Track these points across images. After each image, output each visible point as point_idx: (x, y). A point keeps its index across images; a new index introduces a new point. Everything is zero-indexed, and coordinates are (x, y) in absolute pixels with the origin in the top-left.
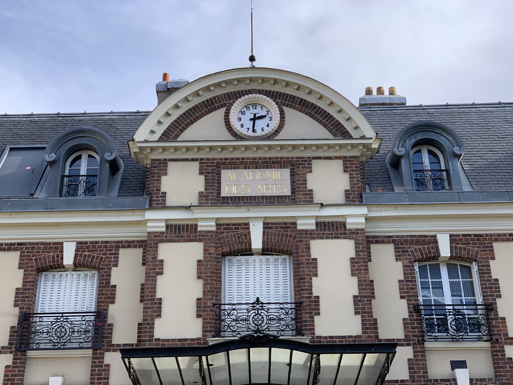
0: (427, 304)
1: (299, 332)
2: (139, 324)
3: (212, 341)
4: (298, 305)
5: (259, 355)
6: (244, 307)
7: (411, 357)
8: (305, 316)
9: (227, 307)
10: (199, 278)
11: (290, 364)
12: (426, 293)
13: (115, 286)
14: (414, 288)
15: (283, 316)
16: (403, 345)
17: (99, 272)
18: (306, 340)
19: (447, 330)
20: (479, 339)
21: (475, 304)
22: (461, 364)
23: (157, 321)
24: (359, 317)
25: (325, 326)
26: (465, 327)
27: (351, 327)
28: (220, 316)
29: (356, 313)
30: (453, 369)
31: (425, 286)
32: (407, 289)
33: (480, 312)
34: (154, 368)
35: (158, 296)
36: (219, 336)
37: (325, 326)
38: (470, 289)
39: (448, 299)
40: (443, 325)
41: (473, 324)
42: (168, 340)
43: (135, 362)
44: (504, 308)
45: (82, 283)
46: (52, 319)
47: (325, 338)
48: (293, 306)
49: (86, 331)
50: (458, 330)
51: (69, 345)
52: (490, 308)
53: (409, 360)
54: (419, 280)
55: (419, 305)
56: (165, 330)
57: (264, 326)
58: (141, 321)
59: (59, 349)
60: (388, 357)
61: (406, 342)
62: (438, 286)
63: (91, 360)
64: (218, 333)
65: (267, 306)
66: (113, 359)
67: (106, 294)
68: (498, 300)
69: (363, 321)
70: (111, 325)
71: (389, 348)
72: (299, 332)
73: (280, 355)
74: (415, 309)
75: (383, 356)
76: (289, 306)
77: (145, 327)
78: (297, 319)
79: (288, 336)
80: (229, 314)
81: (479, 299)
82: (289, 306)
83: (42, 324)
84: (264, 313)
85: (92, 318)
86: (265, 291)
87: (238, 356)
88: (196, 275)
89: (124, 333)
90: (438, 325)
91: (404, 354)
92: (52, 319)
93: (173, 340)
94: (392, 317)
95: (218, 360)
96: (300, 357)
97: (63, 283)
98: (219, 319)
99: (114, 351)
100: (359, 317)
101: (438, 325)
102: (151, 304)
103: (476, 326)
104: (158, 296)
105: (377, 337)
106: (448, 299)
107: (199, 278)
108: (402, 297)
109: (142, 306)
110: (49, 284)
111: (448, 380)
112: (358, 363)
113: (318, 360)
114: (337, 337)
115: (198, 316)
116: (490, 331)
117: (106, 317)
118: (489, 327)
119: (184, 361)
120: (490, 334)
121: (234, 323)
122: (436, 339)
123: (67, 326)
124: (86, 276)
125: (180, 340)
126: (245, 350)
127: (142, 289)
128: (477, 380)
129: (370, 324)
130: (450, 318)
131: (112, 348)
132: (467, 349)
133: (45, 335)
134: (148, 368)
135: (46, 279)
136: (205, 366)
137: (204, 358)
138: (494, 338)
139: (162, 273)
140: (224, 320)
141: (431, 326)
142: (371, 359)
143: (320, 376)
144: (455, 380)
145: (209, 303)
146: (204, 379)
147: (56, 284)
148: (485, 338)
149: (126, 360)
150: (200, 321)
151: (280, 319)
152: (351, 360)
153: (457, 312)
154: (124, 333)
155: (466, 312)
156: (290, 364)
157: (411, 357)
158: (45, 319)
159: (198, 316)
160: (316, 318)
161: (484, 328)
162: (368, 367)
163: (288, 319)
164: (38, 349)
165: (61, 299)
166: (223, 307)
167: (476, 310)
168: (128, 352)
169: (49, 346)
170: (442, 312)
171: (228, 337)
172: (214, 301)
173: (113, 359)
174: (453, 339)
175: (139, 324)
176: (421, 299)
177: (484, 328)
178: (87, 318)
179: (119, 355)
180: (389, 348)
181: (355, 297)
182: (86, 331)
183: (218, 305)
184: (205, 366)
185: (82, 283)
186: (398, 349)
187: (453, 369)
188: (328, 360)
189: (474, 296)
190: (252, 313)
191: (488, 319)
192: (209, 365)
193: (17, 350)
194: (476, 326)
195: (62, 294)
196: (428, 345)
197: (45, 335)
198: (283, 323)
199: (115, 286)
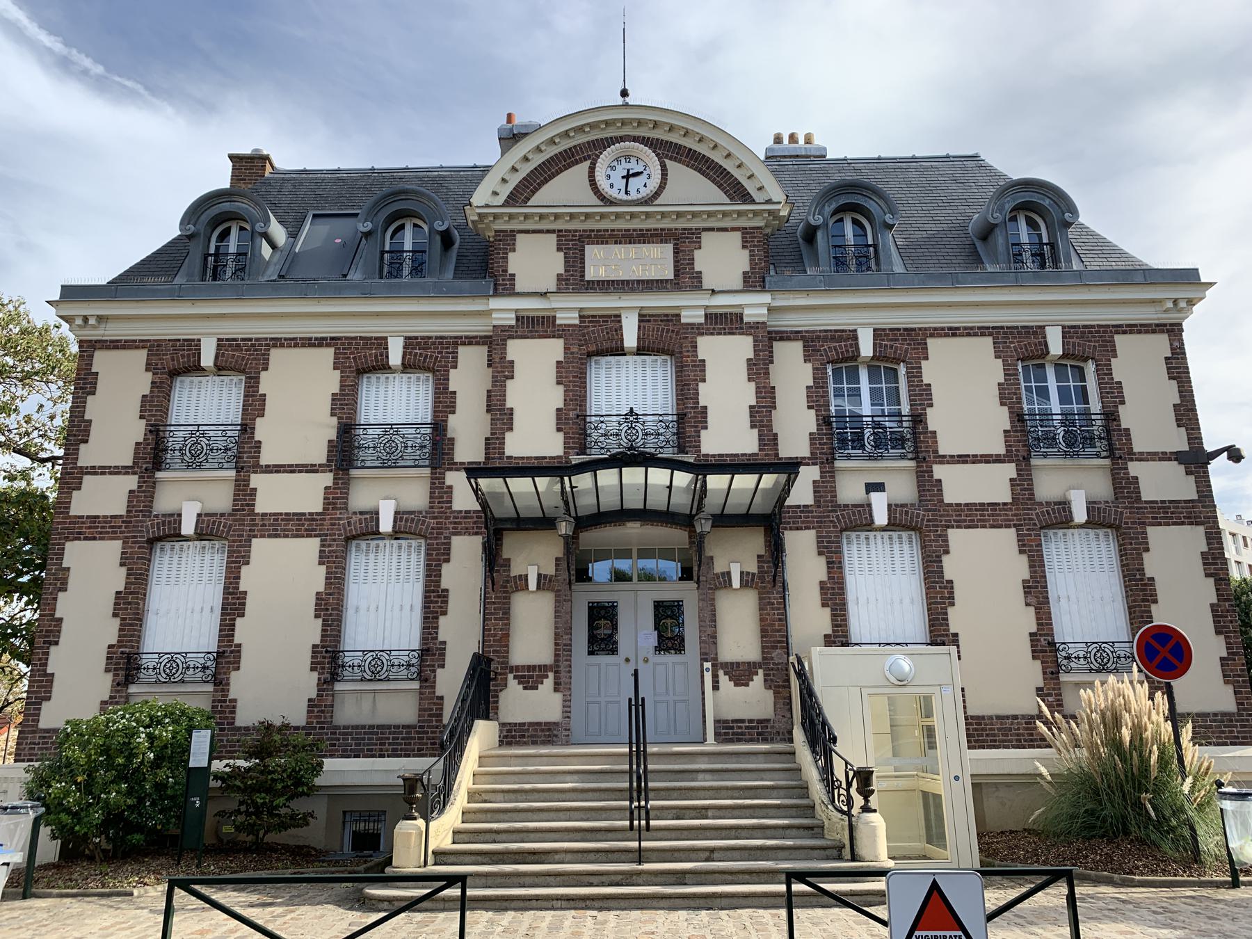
0: (841, 415)
1: (682, 449)
2: (487, 439)
3: (575, 459)
4: (681, 417)
5: (633, 475)
6: (615, 419)
7: (818, 478)
8: (690, 431)
9: (593, 419)
10: (558, 383)
11: (670, 487)
12: (839, 401)
13: (455, 393)
14: (825, 395)
15: (662, 431)
16: (808, 464)
17: (434, 375)
18: (690, 458)
19: (863, 447)
20: (903, 457)
21: (899, 414)
22: (879, 487)
23: (508, 435)
24: (756, 431)
25: (713, 443)
26: (886, 442)
27: (746, 443)
28: (585, 430)
29: (752, 427)
30: (868, 492)
31: (839, 394)
32: (816, 397)
33: (905, 424)
34: (505, 490)
35: (508, 405)
36: (585, 454)
37: (713, 443)
38: (895, 397)
39: (866, 408)
40: (858, 441)
41: (896, 439)
42: (523, 458)
43: (484, 483)
44: (935, 419)
45: (413, 388)
46: (379, 431)
47: (714, 456)
48: (675, 418)
49: (422, 447)
50: (876, 447)
51: (402, 463)
52: (918, 419)
53: (814, 482)
54: (831, 386)
55: (830, 417)
56: (517, 446)
57: (639, 442)
58: (489, 435)
59: (390, 467)
60: (789, 478)
61: (812, 461)
62: (855, 394)
63: (429, 480)
64: (583, 450)
65: (643, 418)
66: (456, 479)
67: (444, 402)
68: (928, 410)
69: (760, 435)
70: (453, 439)
71: (790, 467)
72: (682, 449)
73: (659, 476)
74: (825, 421)
75: (783, 477)
76: (670, 418)
77: (494, 443)
78: (679, 434)
79: (668, 453)
80: (596, 428)
81: (905, 409)
82: (670, 418)
83: (367, 438)
84: (639, 427)
85: (429, 431)
86: (640, 400)
87: (607, 477)
88: (555, 381)
89: (469, 448)
90: (853, 441)
91: (809, 475)
92: (379, 431)
93: (528, 458)
94: (796, 430)
95: (583, 481)
96: (682, 479)
97: (390, 387)
98: (584, 434)
99: (457, 470)
100: (756, 431)
101: (853, 441)
102: (500, 416)
103: (899, 441)
104: (508, 405)
105: (777, 455)
106: (866, 408)
107: (558, 383)
108: (809, 407)
109: (489, 417)
110: (373, 389)
111: (862, 506)
112: (753, 486)
113: (704, 482)
114: (727, 455)
115: (559, 430)
116: (916, 447)
117: (445, 430)
118: (915, 442)
119: (543, 482)
120: (916, 451)
121: (602, 439)
122: (849, 457)
123: (398, 439)
124: (418, 379)
125: (536, 458)
126: (616, 471)
127: (489, 397)
128: (896, 505)
129: (769, 439)
130: (867, 433)
131: (454, 466)
132: (887, 469)
133: (371, 451)
134: (498, 490)
135: (369, 383)
136: (568, 489)
137: (566, 479)
138: (921, 455)
139: (512, 377)
140: (590, 435)
141: (843, 442)
142: (768, 480)
143: (706, 501)
144: (869, 505)
145: (572, 414)
146: (566, 503)
147: (382, 389)
148: (910, 456)
149: (473, 481)
150: (561, 436)
151: (658, 434)
152: (745, 482)
153: (877, 425)
154: (469, 448)
155: (887, 424)
156: (670, 487)
157: (818, 478)
158: (370, 431)
159: (559, 430)
160: (703, 433)
161: (909, 443)
162: (765, 490)
163: (669, 434)
164: (363, 467)
165: (389, 408)
166: (588, 419)
167: (901, 421)
168: (474, 471)
169: (377, 464)
170: (859, 425)
171: (596, 454)
172: (577, 412)
173: (456, 479)
174: (870, 457)
175: (487, 439)
176: (833, 409)
177: (909, 443)
178: (423, 431)
179: (463, 474)
180: (790, 467)
181: (751, 407)
182: (422, 447)
183: (583, 417)
184: (568, 489)
185: (413, 388)
186: (802, 469)
187: (868, 492)
188: (716, 482)
189: (899, 404)
190: (624, 427)
191: (914, 433)
192: (572, 487)
193: (338, 469)
194: (899, 441)
195: (390, 402)
196: (838, 464)
197: (371, 451)
198: (662, 438)
199: (455, 393)
